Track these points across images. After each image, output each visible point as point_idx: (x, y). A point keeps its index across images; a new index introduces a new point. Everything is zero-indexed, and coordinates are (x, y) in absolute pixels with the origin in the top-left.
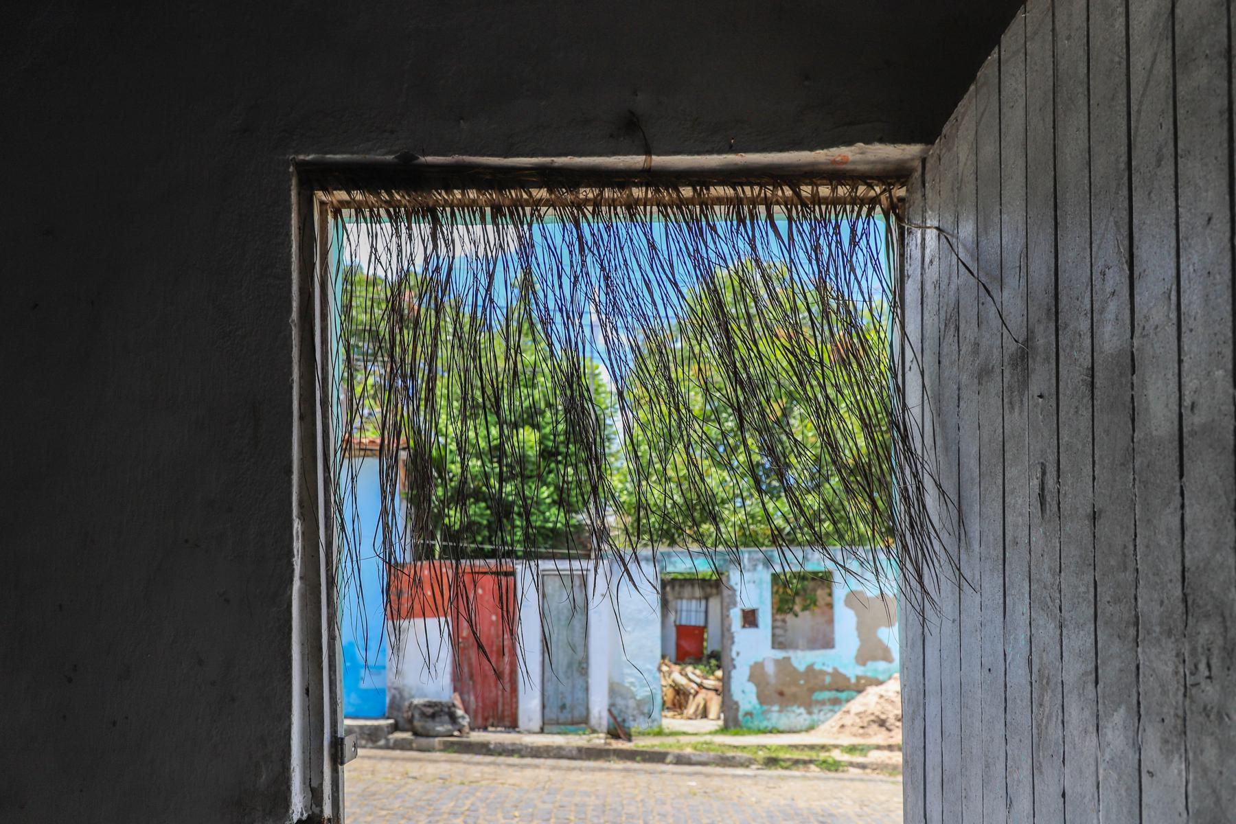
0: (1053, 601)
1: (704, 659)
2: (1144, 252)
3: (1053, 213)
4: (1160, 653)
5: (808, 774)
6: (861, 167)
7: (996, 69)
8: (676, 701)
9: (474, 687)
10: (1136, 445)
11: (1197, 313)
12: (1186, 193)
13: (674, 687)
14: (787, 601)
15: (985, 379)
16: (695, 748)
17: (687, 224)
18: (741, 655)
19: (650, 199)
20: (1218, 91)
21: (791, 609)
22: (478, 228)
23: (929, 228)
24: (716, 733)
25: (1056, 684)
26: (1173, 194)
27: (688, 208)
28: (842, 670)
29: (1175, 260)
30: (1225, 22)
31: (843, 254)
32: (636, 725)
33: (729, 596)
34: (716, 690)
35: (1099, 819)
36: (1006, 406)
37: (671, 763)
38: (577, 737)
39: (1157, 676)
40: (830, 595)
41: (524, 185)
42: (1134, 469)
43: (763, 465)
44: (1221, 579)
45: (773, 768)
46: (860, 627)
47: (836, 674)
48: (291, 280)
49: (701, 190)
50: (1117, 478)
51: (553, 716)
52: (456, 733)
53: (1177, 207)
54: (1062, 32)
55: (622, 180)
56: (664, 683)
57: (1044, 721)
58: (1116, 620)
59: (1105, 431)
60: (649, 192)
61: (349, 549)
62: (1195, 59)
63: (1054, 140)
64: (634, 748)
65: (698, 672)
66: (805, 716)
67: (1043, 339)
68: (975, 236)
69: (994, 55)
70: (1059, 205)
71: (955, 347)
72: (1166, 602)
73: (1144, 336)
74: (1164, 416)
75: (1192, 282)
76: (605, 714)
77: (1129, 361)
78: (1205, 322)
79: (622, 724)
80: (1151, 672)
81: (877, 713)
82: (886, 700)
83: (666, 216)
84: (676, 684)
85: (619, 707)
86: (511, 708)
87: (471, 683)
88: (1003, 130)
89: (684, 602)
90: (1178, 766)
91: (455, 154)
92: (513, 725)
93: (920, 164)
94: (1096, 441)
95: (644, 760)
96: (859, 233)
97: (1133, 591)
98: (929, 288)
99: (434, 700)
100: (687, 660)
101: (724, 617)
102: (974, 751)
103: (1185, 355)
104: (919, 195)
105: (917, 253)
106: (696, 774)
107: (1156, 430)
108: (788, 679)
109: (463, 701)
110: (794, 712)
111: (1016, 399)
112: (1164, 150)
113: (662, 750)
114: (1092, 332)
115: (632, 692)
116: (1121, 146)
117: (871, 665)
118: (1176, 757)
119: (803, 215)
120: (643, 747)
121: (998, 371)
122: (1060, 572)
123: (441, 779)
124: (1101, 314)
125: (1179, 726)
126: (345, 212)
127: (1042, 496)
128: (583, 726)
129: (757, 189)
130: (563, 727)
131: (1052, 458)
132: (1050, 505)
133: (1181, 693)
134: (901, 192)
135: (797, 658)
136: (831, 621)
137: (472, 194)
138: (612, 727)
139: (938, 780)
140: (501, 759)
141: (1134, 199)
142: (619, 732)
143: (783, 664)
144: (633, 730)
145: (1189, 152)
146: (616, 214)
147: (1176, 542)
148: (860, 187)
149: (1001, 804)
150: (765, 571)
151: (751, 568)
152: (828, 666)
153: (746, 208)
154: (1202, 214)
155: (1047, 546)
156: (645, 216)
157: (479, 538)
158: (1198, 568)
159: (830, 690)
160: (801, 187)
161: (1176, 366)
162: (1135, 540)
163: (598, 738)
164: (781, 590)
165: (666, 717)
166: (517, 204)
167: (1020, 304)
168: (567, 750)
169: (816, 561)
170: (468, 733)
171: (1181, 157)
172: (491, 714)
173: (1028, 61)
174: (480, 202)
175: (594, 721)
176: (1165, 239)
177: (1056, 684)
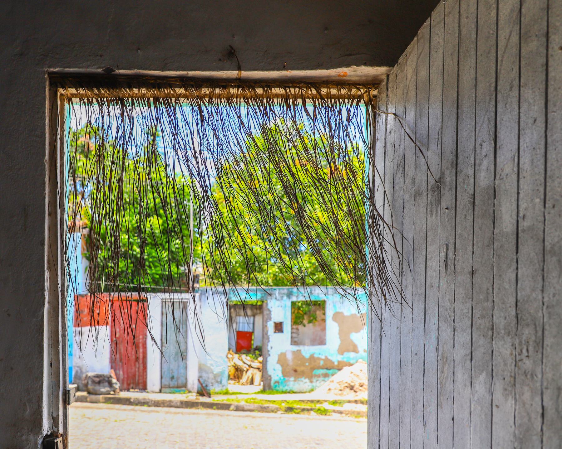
0: (450, 317)
1: (252, 350)
2: (501, 135)
3: (456, 111)
4: (504, 344)
5: (310, 417)
6: (354, 79)
7: (429, 30)
8: (236, 375)
9: (123, 366)
10: (495, 236)
11: (527, 168)
12: (524, 107)
13: (234, 367)
14: (299, 318)
15: (418, 198)
16: (247, 402)
17: (259, 108)
18: (273, 348)
19: (240, 95)
20: (542, 54)
21: (302, 322)
22: (146, 109)
23: (389, 113)
24: (258, 393)
25: (451, 361)
26: (518, 106)
27: (260, 100)
28: (330, 358)
29: (517, 140)
30: (546, 18)
31: (343, 126)
32: (213, 389)
33: (267, 314)
34: (259, 369)
35: (470, 431)
36: (429, 213)
37: (233, 410)
38: (180, 395)
39: (502, 356)
40: (324, 314)
41: (171, 86)
42: (493, 248)
43: (287, 239)
44: (535, 306)
45: (290, 413)
46: (341, 333)
47: (327, 360)
48: (45, 138)
49: (267, 90)
50: (485, 253)
51: (167, 383)
52: (112, 393)
53: (519, 113)
54: (464, 14)
55: (225, 84)
56: (229, 364)
57: (444, 381)
58: (482, 327)
59: (479, 228)
60: (239, 91)
61: (73, 287)
62: (530, 37)
63: (458, 72)
64: (212, 402)
65: (248, 358)
66: (309, 384)
67: (449, 178)
68: (415, 120)
69: (427, 23)
70: (459, 107)
71: (402, 180)
72: (508, 317)
73: (501, 179)
74: (509, 221)
75: (526, 152)
76: (196, 382)
77: (493, 192)
78: (531, 173)
79: (205, 388)
80: (499, 354)
81: (349, 382)
82: (355, 374)
83: (248, 104)
84: (236, 365)
85: (204, 378)
86: (143, 378)
87: (121, 364)
88: (431, 64)
89: (241, 318)
90: (511, 401)
91: (135, 69)
92: (144, 388)
93: (386, 78)
94: (475, 233)
95: (218, 408)
96: (352, 114)
97: (491, 312)
98: (389, 146)
99: (100, 373)
100: (242, 351)
101: (264, 327)
102: (407, 397)
103: (521, 190)
104: (384, 95)
105: (383, 127)
106: (247, 416)
107: (505, 228)
108: (299, 362)
109: (116, 374)
110: (302, 381)
111: (434, 209)
112: (514, 82)
113: (228, 402)
114: (475, 176)
115: (212, 370)
116: (492, 78)
117: (346, 354)
118: (510, 397)
119: (322, 105)
120: (217, 401)
121: (425, 194)
122: (454, 302)
123: (104, 418)
124: (479, 166)
125: (512, 382)
126: (74, 100)
127: (446, 262)
128: (184, 389)
129: (297, 90)
130: (172, 389)
131: (452, 241)
132: (450, 267)
133: (513, 365)
134: (374, 92)
135: (304, 350)
136: (324, 329)
137: (144, 91)
138: (200, 389)
139: (387, 414)
140: (138, 407)
141: (498, 107)
142: (204, 392)
143: (297, 354)
144: (212, 391)
145: (526, 85)
146: (221, 102)
147: (514, 287)
148: (353, 89)
149: (421, 424)
150: (288, 300)
151: (280, 299)
152: (322, 355)
153: (291, 100)
154: (532, 117)
155: (448, 288)
156: (237, 104)
157: (126, 280)
158: (524, 300)
159: (323, 369)
160: (321, 89)
161: (516, 195)
162: (493, 285)
163: (192, 395)
164: (296, 311)
165: (230, 384)
166: (168, 96)
167: (438, 159)
168: (175, 402)
169: (318, 293)
170: (119, 393)
171: (522, 87)
172: (132, 381)
173: (446, 28)
174: (147, 95)
175: (189, 386)
176: (513, 129)
177: (451, 361)
